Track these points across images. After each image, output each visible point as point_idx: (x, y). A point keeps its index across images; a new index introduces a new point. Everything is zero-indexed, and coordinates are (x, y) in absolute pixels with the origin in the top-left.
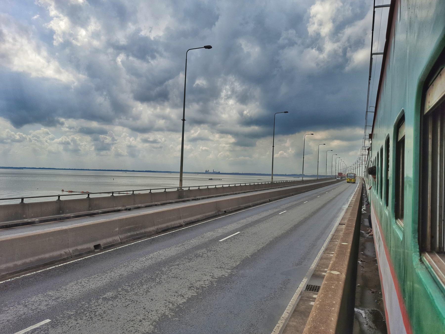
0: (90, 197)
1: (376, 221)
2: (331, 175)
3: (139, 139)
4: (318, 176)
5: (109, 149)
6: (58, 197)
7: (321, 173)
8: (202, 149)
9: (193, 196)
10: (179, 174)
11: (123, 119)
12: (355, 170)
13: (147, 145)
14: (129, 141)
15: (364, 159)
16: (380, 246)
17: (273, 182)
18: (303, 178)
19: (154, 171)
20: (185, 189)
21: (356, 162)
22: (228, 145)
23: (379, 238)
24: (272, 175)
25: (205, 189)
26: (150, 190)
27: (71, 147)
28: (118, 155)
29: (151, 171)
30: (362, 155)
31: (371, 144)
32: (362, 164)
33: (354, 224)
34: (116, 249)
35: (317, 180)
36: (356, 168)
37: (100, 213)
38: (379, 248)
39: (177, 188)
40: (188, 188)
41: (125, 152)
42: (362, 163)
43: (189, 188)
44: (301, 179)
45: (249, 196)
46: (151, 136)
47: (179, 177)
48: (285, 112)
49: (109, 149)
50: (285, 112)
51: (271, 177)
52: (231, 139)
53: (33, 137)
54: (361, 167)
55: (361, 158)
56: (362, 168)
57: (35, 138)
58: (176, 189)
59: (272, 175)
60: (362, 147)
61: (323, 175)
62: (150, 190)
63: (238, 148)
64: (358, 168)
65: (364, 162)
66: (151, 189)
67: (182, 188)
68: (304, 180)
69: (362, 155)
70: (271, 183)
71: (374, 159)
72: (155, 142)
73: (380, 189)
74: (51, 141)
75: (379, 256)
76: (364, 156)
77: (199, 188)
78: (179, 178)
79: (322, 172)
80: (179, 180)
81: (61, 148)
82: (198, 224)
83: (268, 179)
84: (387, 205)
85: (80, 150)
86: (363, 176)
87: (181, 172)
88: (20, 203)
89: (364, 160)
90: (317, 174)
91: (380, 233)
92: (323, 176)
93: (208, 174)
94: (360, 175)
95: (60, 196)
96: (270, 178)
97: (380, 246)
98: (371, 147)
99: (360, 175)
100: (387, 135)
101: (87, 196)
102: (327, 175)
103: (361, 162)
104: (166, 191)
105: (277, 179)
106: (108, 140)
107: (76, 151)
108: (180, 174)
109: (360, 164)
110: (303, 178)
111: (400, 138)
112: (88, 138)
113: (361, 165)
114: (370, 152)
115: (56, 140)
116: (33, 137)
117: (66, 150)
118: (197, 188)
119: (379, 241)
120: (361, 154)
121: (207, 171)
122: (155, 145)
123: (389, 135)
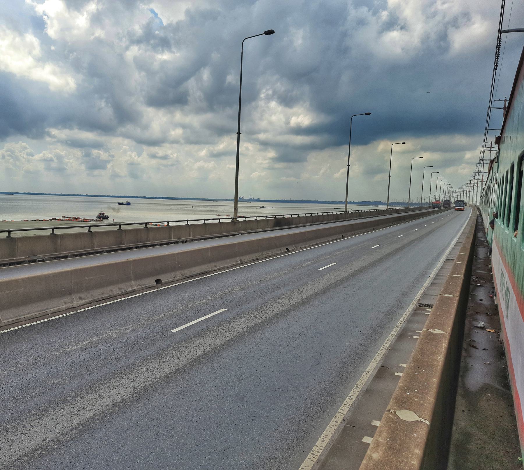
0: (91, 230)
1: (502, 267)
2: (420, 202)
3: (145, 154)
4: (409, 204)
5: (104, 168)
6: (52, 230)
7: (414, 200)
8: (229, 167)
9: (270, 226)
10: (234, 202)
11: (129, 128)
12: (462, 196)
13: (154, 162)
14: (131, 156)
15: (480, 177)
16: (507, 303)
17: (348, 212)
18: (388, 207)
19: (105, 196)
20: (240, 220)
21: (468, 183)
22: (267, 161)
23: (508, 290)
24: (346, 203)
25: (115, 231)
26: (187, 222)
27: (54, 165)
28: (115, 176)
29: (167, 197)
30: (478, 173)
31: (498, 153)
32: (477, 186)
33: (452, 320)
34: (20, 327)
35: (409, 210)
36: (468, 192)
37: (3, 265)
38: (506, 304)
39: (119, 226)
40: (119, 226)
41: (123, 171)
42: (478, 185)
43: (219, 221)
44: (386, 207)
45: (305, 233)
46: (160, 151)
47: (234, 205)
48: (366, 114)
49: (104, 168)
50: (366, 114)
51: (344, 205)
52: (272, 154)
53: (6, 151)
54: (475, 191)
55: (477, 177)
56: (477, 192)
57: (9, 153)
58: (230, 220)
59: (346, 203)
60: (479, 160)
61: (403, 203)
62: (187, 222)
63: (280, 165)
64: (470, 191)
65: (480, 184)
66: (189, 219)
67: (238, 219)
68: (390, 209)
69: (478, 173)
70: (233, 221)
71: (501, 178)
72: (165, 157)
73: (503, 214)
74: (29, 156)
75: (505, 316)
76: (481, 174)
77: (187, 224)
78: (234, 207)
79: (415, 198)
80: (234, 208)
81: (41, 166)
82: (176, 284)
83: (341, 208)
84: (508, 226)
85: (66, 169)
86: (478, 202)
87: (236, 201)
88: (118, 229)
89: (481, 180)
90: (407, 202)
91: (509, 283)
92: (418, 204)
93: (243, 201)
94: (476, 202)
95: (11, 232)
96: (343, 207)
97: (507, 303)
98: (496, 158)
99: (476, 202)
100: (512, 162)
101: (6, 234)
102: (431, 201)
103: (476, 182)
104: (246, 220)
105: (351, 208)
106: (103, 155)
107: (61, 170)
108: (234, 202)
109: (474, 186)
110: (388, 207)
111: (522, 170)
112: (78, 152)
113: (475, 188)
114: (495, 165)
115: (37, 157)
116: (6, 151)
117: (48, 168)
118: (185, 223)
119: (507, 295)
120: (477, 171)
121: (242, 197)
122: (164, 162)
123: (514, 162)
